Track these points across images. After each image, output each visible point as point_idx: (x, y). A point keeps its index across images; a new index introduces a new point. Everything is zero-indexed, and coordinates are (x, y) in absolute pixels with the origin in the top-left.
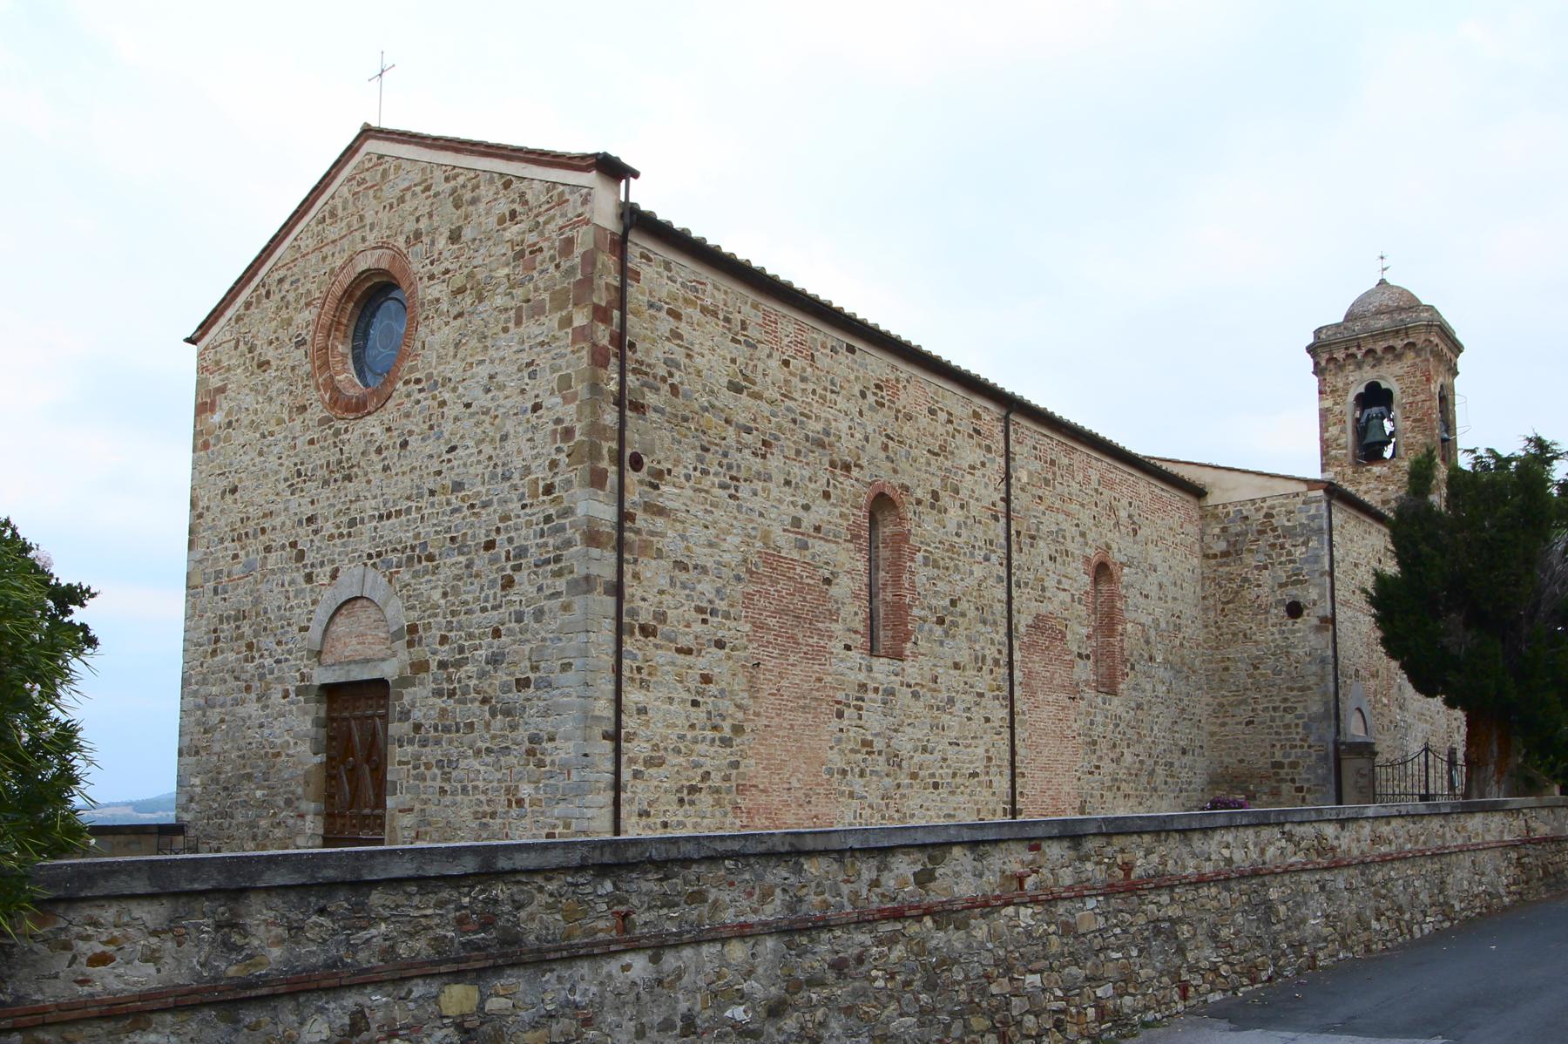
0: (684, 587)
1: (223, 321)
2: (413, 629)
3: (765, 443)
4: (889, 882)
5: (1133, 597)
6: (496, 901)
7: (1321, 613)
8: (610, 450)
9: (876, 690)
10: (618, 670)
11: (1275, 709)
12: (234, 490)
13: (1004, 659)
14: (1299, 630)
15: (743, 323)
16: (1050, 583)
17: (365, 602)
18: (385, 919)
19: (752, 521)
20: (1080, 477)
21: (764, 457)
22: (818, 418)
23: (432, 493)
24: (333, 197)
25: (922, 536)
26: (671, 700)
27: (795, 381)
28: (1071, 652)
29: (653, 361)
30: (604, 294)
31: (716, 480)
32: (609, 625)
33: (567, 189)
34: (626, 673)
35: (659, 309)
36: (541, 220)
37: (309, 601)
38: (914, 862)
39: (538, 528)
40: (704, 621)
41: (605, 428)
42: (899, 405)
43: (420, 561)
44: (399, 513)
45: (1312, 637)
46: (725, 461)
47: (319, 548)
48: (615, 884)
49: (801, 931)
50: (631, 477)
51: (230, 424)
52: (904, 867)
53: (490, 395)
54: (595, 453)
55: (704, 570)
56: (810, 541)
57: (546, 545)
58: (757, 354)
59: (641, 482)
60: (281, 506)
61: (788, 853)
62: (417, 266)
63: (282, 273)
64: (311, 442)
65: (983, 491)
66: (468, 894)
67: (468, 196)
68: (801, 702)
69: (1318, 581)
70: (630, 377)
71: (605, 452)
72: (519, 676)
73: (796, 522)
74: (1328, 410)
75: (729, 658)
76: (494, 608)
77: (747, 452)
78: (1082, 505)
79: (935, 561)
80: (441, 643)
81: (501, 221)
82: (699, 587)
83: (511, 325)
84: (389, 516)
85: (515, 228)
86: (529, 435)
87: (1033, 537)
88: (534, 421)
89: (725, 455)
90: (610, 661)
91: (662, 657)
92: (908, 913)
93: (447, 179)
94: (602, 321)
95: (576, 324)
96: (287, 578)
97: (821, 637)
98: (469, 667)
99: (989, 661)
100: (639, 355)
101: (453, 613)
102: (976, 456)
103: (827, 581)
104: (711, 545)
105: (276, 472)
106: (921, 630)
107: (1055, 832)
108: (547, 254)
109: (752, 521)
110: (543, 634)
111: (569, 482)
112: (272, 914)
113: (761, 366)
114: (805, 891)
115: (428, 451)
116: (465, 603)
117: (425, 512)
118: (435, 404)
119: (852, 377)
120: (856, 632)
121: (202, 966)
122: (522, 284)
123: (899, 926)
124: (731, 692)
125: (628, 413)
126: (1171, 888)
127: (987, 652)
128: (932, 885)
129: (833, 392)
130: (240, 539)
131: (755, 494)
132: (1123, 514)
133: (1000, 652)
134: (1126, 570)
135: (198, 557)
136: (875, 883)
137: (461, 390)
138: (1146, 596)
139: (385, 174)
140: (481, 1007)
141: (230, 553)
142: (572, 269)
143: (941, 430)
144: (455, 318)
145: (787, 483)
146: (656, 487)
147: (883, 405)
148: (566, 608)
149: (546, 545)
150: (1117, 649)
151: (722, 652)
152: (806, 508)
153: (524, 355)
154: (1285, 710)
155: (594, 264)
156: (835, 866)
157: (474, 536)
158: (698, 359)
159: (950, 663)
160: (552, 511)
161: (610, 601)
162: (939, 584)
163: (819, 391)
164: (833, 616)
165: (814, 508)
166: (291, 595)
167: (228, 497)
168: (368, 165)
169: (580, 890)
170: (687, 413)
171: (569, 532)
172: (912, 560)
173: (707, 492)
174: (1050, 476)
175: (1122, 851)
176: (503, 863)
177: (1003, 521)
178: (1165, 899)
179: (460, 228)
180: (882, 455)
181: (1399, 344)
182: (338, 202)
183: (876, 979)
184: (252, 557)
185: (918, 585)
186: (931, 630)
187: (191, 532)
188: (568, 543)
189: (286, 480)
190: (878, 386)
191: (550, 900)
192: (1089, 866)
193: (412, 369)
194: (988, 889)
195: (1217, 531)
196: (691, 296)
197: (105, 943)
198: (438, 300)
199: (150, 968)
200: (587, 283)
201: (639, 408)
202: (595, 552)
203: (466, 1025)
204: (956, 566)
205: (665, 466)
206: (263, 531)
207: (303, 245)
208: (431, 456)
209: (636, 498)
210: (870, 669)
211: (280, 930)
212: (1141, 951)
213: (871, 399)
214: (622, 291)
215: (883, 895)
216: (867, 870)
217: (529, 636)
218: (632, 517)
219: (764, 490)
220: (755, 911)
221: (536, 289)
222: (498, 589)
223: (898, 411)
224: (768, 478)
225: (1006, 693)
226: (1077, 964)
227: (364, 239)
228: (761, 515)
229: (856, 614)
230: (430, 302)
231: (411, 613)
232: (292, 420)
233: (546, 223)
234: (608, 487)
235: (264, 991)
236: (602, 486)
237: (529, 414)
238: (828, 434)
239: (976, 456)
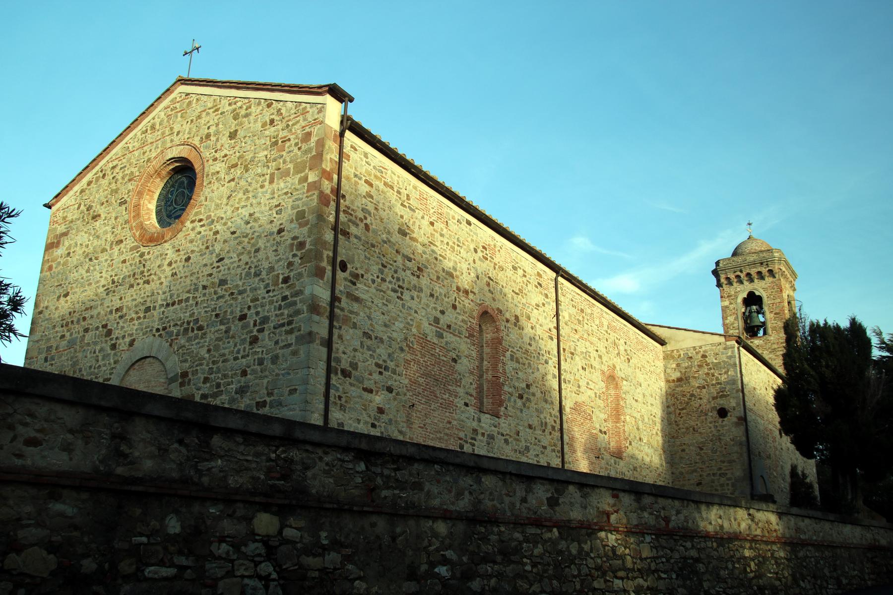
0: (369, 349)
1: (71, 193)
2: (184, 375)
3: (419, 268)
4: (532, 501)
5: (629, 400)
6: (292, 461)
7: (738, 415)
8: (328, 256)
9: (483, 434)
10: (327, 395)
11: (714, 474)
12: (66, 295)
13: (558, 426)
14: (726, 426)
15: (408, 196)
16: (583, 383)
17: (151, 360)
18: (221, 457)
19: (410, 315)
20: (597, 322)
21: (418, 277)
22: (450, 260)
23: (205, 287)
24: (154, 119)
25: (510, 342)
26: (359, 421)
27: (437, 235)
28: (595, 429)
29: (355, 208)
30: (329, 164)
31: (390, 286)
32: (322, 365)
33: (308, 105)
34: (332, 399)
35: (360, 179)
36: (290, 123)
37: (112, 361)
38: (547, 491)
39: (277, 305)
40: (380, 373)
41: (325, 242)
42: (496, 260)
43: (193, 331)
44: (180, 302)
45: (733, 429)
46: (395, 276)
47: (123, 327)
48: (367, 467)
49: (481, 522)
50: (340, 275)
51: (69, 254)
52: (541, 492)
53: (249, 226)
54: (318, 256)
55: (382, 341)
56: (445, 334)
57: (282, 314)
58: (416, 214)
59: (345, 279)
60: (99, 303)
61: (473, 468)
62: (206, 154)
63: (115, 163)
64: (124, 262)
65: (544, 321)
66: (275, 452)
67: (243, 112)
68: (438, 435)
69: (735, 395)
70: (342, 215)
71: (325, 256)
72: (258, 400)
73: (437, 320)
74: (727, 307)
75: (395, 399)
76: (242, 357)
77: (408, 272)
78: (599, 339)
79: (517, 358)
80: (204, 382)
81: (264, 125)
82: (378, 351)
83: (267, 184)
84: (173, 304)
85: (273, 129)
86: (274, 248)
87: (572, 354)
88: (278, 239)
89: (396, 272)
90: (322, 389)
91: (354, 392)
92: (544, 523)
93: (230, 104)
94: (327, 179)
95: (310, 180)
96: (98, 348)
97: (451, 395)
98: (223, 397)
99: (549, 427)
100: (347, 203)
101: (214, 363)
102: (540, 299)
103: (454, 360)
104: (386, 326)
105: (98, 282)
106: (509, 400)
107: (627, 487)
108: (293, 142)
109: (410, 315)
110: (277, 371)
111: (300, 275)
112: (149, 436)
113: (417, 223)
114: (482, 496)
115: (204, 262)
116: (224, 355)
117: (199, 300)
118: (212, 233)
119: (469, 240)
120: (471, 395)
121: (100, 462)
122: (275, 160)
123: (539, 531)
124: (396, 421)
125: (340, 236)
126: (692, 537)
127: (548, 421)
128: (557, 508)
129: (458, 246)
130: (67, 325)
131: (413, 298)
132: (622, 348)
133: (555, 422)
134: (625, 382)
135: (36, 339)
136: (524, 500)
137: (229, 224)
138: (636, 401)
139: (190, 103)
140: (280, 532)
141: (59, 335)
142: (309, 150)
143: (519, 280)
144: (229, 182)
145: (432, 295)
146: (354, 284)
147: (487, 259)
148: (295, 353)
149: (282, 314)
150: (622, 431)
151: (390, 395)
152: (443, 312)
153: (275, 200)
154: (720, 475)
155: (323, 146)
156: (501, 483)
157: (232, 313)
158: (381, 212)
159: (526, 424)
160: (287, 293)
161: (324, 350)
162: (520, 373)
163: (451, 243)
164: (458, 383)
165: (447, 313)
166: (100, 358)
167: (62, 299)
168: (178, 99)
169: (345, 465)
170: (374, 242)
171: (299, 306)
172: (504, 356)
173: (384, 292)
174: (581, 319)
175: (664, 509)
176: (298, 434)
177: (555, 340)
178: (689, 545)
179: (236, 131)
180: (486, 288)
181: (764, 270)
182: (157, 121)
183: (526, 564)
184: (74, 336)
185: (507, 371)
186: (515, 401)
187: (33, 323)
188: (298, 312)
189: (104, 286)
190: (484, 247)
191: (327, 468)
192: (646, 515)
193: (197, 214)
194: (590, 518)
195: (674, 366)
196: (379, 174)
197: (38, 431)
198: (218, 172)
199: (65, 456)
200: (319, 156)
201: (346, 234)
202: (316, 318)
203: (271, 543)
204: (529, 364)
205: (360, 272)
206: (84, 319)
207: (131, 146)
208: (206, 265)
209: (342, 288)
210: (479, 420)
211: (153, 448)
212: (678, 576)
213: (480, 254)
214: (340, 163)
215: (529, 509)
216: (520, 490)
217: (267, 373)
218: (339, 300)
219: (418, 297)
220: (453, 504)
221: (284, 162)
222: (247, 346)
223: (495, 264)
224: (421, 290)
225: (559, 448)
226: (642, 577)
227: (172, 141)
228: (416, 312)
229: (471, 384)
230: (213, 174)
231: (184, 364)
232: (111, 248)
233: (293, 125)
234: (325, 278)
235: (140, 488)
236: (322, 278)
237: (275, 235)
238: (455, 270)
239: (540, 299)
